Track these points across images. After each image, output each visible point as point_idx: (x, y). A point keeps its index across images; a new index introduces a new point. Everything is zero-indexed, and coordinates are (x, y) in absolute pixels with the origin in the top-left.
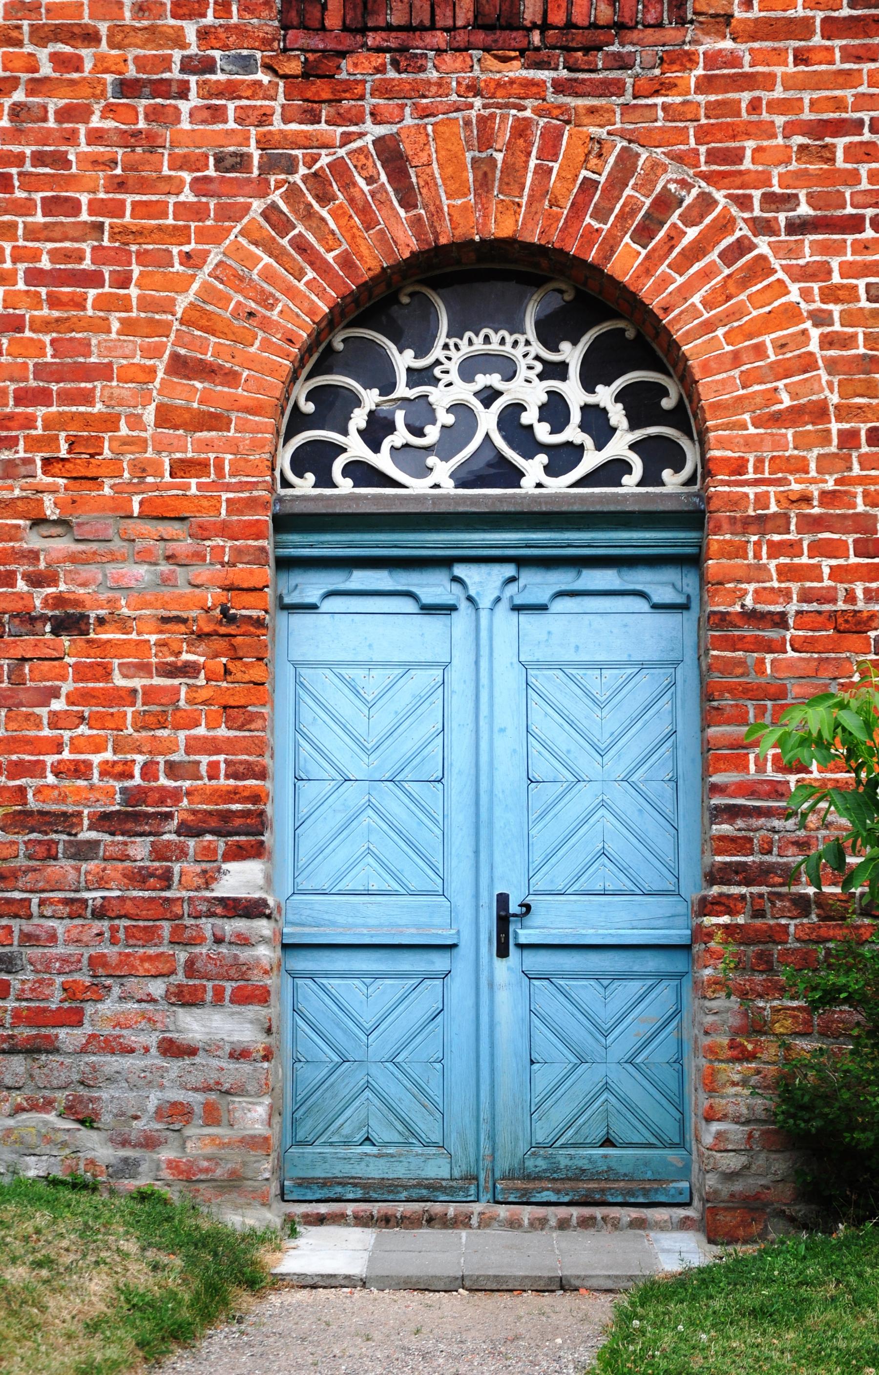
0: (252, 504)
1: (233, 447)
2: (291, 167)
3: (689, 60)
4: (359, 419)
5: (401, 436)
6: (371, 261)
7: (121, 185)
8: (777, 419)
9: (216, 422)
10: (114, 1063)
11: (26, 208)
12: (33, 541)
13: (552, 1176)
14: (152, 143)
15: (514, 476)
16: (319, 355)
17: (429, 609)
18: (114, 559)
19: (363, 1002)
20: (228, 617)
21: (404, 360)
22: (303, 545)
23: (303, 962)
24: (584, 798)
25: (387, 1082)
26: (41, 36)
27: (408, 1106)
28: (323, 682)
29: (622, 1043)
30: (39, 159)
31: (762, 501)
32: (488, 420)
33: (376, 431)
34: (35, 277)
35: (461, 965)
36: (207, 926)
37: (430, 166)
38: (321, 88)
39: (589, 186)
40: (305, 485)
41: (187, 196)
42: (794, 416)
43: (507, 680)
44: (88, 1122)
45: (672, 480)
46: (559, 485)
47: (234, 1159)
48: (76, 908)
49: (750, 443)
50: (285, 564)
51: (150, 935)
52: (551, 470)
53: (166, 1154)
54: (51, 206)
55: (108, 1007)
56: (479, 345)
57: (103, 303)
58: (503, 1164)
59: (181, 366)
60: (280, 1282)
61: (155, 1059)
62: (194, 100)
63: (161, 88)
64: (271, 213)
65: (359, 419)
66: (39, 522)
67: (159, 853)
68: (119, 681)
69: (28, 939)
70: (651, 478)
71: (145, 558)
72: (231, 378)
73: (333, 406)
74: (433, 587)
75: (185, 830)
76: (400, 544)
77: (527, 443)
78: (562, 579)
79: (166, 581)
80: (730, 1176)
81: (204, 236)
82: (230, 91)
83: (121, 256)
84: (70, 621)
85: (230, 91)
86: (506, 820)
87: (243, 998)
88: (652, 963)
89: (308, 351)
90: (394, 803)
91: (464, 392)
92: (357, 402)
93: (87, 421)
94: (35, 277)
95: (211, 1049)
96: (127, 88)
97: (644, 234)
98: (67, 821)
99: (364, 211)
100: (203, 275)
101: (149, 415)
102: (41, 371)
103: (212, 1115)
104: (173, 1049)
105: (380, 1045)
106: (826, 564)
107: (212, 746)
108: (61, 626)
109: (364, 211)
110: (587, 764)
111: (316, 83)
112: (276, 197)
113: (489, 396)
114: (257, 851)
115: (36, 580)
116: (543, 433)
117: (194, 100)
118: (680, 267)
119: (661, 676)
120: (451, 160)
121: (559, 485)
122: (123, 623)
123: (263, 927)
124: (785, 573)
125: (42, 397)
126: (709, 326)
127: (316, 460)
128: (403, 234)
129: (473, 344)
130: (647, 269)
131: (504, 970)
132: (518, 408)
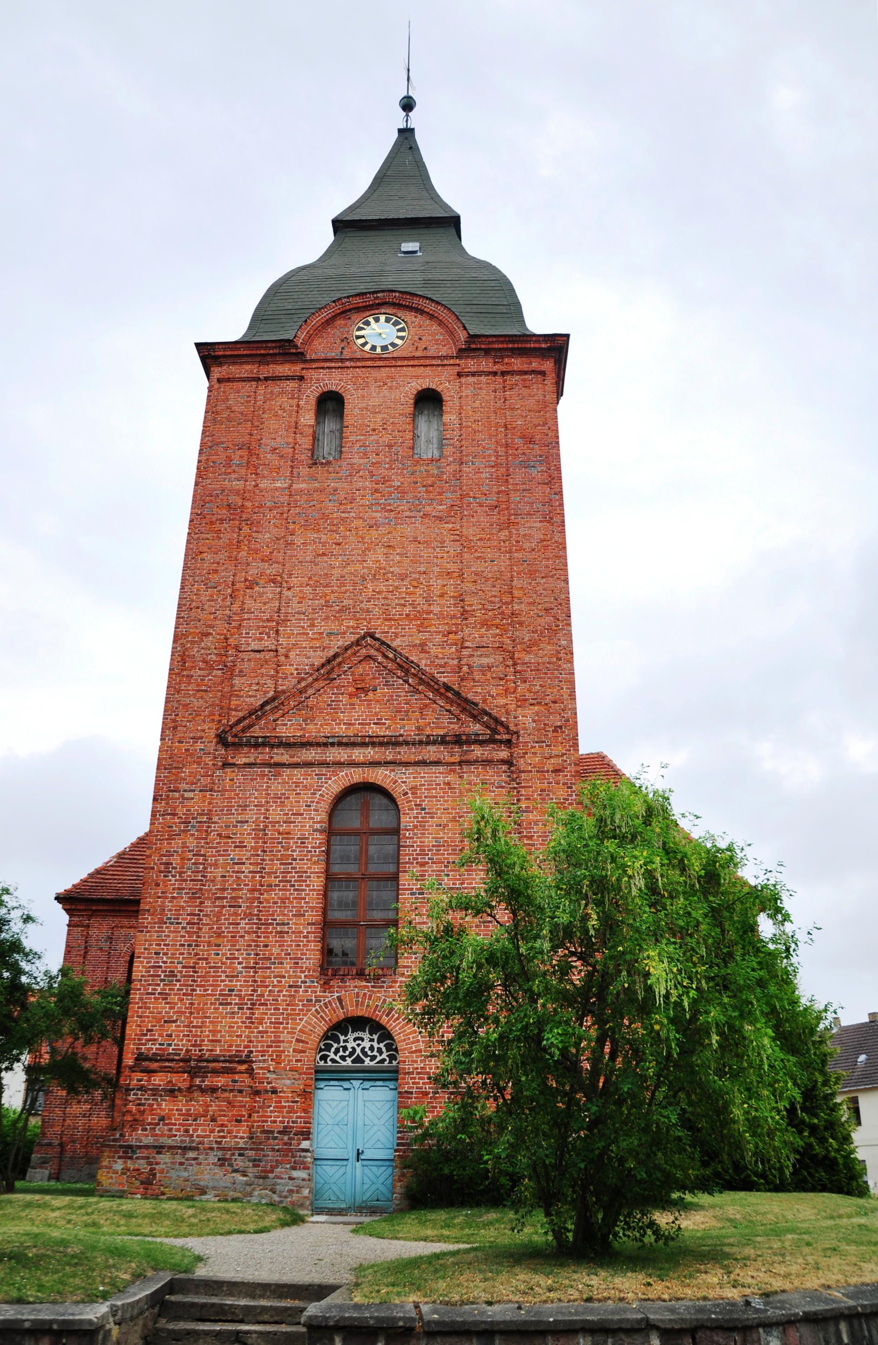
0: (310, 1068)
1: (307, 1057)
2: (320, 1001)
3: (397, 982)
4: (333, 1050)
5: (341, 1053)
6: (335, 1020)
7: (288, 1005)
8: (412, 1052)
9: (304, 1052)
10: (279, 1181)
11: (270, 1009)
12: (268, 1075)
13: (366, 1207)
14: (294, 996)
15: (363, 1062)
16: (326, 1036)
17: (345, 1089)
18: (283, 1079)
19: (329, 1173)
20: (305, 1091)
21: (342, 1038)
22: (320, 1076)
23: (318, 1162)
24: (375, 1129)
25: (334, 1188)
26: (275, 977)
27: (338, 1193)
28: (323, 1104)
29: (381, 1180)
30: (273, 1000)
31: (409, 1069)
32: (358, 1050)
33: (337, 1051)
34: (271, 1023)
35: (350, 1163)
36: (298, 1154)
37: (347, 1001)
38: (327, 986)
39: (377, 1006)
40: (322, 1063)
41: (301, 1007)
42: (416, 1052)
43: (361, 1103)
44: (274, 1193)
45: (394, 1063)
46: (372, 1063)
47: (302, 1200)
48: (273, 1150)
49: (407, 1057)
50: (317, 1080)
51: (287, 1155)
52: (371, 1060)
53: (289, 1199)
54: (275, 1009)
55: (278, 1170)
56: (357, 1035)
57: (283, 1028)
58: (357, 1205)
59: (298, 1040)
60: (307, 1222)
61: (287, 1180)
62: (303, 989)
63: (296, 986)
64: (316, 1010)
65: (333, 1050)
66: (269, 1071)
67: (290, 1139)
68: (283, 1104)
69: (264, 1156)
70: (390, 1062)
71: (289, 1079)
72: (307, 1043)
73: (328, 1047)
74: (346, 1085)
75: (295, 1134)
76: (339, 1075)
77: (366, 1055)
78: (372, 1083)
79: (293, 1083)
80: (397, 1205)
81: (303, 1015)
82: (310, 987)
83: (287, 1019)
84: (274, 1092)
85: (310, 987)
86: (359, 1133)
87: (304, 1168)
88: (388, 1163)
89: (322, 1037)
90: (337, 1129)
91: (354, 1044)
92: (332, 1046)
93: (279, 1051)
94: (271, 1023)
95: (298, 1179)
96: (290, 986)
97: (387, 1015)
98: (272, 1132)
99: (334, 1010)
100: (303, 1022)
101: (291, 1050)
102: (271, 1041)
103: (298, 1192)
104: (291, 1178)
105: (333, 1180)
106: (421, 1081)
107: (300, 1117)
108: (273, 1092)
109: (334, 1010)
110: (376, 1122)
111: (326, 986)
112: (317, 1007)
113: (359, 1045)
114: (308, 1139)
115: (268, 1083)
116: (369, 1053)
117: (303, 989)
118: (394, 1022)
119: (391, 1103)
120: (351, 1000)
121: (372, 1063)
122: (285, 1092)
123: (309, 1154)
124: (413, 1083)
125: (271, 1046)
126: (399, 1034)
127: (324, 1058)
128: (341, 1014)
129: (356, 1035)
130: (388, 1022)
131: (358, 1164)
132: (364, 1048)
